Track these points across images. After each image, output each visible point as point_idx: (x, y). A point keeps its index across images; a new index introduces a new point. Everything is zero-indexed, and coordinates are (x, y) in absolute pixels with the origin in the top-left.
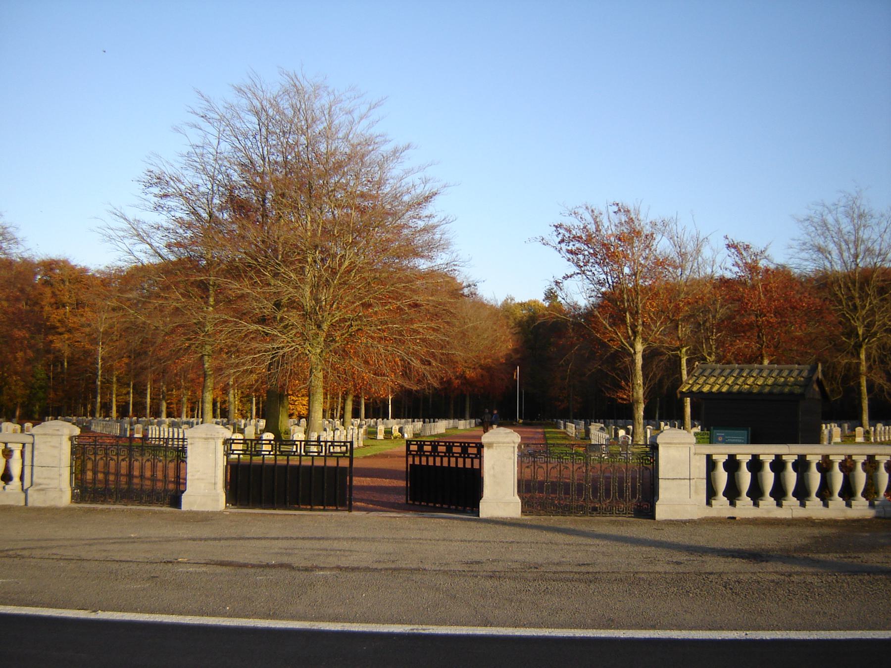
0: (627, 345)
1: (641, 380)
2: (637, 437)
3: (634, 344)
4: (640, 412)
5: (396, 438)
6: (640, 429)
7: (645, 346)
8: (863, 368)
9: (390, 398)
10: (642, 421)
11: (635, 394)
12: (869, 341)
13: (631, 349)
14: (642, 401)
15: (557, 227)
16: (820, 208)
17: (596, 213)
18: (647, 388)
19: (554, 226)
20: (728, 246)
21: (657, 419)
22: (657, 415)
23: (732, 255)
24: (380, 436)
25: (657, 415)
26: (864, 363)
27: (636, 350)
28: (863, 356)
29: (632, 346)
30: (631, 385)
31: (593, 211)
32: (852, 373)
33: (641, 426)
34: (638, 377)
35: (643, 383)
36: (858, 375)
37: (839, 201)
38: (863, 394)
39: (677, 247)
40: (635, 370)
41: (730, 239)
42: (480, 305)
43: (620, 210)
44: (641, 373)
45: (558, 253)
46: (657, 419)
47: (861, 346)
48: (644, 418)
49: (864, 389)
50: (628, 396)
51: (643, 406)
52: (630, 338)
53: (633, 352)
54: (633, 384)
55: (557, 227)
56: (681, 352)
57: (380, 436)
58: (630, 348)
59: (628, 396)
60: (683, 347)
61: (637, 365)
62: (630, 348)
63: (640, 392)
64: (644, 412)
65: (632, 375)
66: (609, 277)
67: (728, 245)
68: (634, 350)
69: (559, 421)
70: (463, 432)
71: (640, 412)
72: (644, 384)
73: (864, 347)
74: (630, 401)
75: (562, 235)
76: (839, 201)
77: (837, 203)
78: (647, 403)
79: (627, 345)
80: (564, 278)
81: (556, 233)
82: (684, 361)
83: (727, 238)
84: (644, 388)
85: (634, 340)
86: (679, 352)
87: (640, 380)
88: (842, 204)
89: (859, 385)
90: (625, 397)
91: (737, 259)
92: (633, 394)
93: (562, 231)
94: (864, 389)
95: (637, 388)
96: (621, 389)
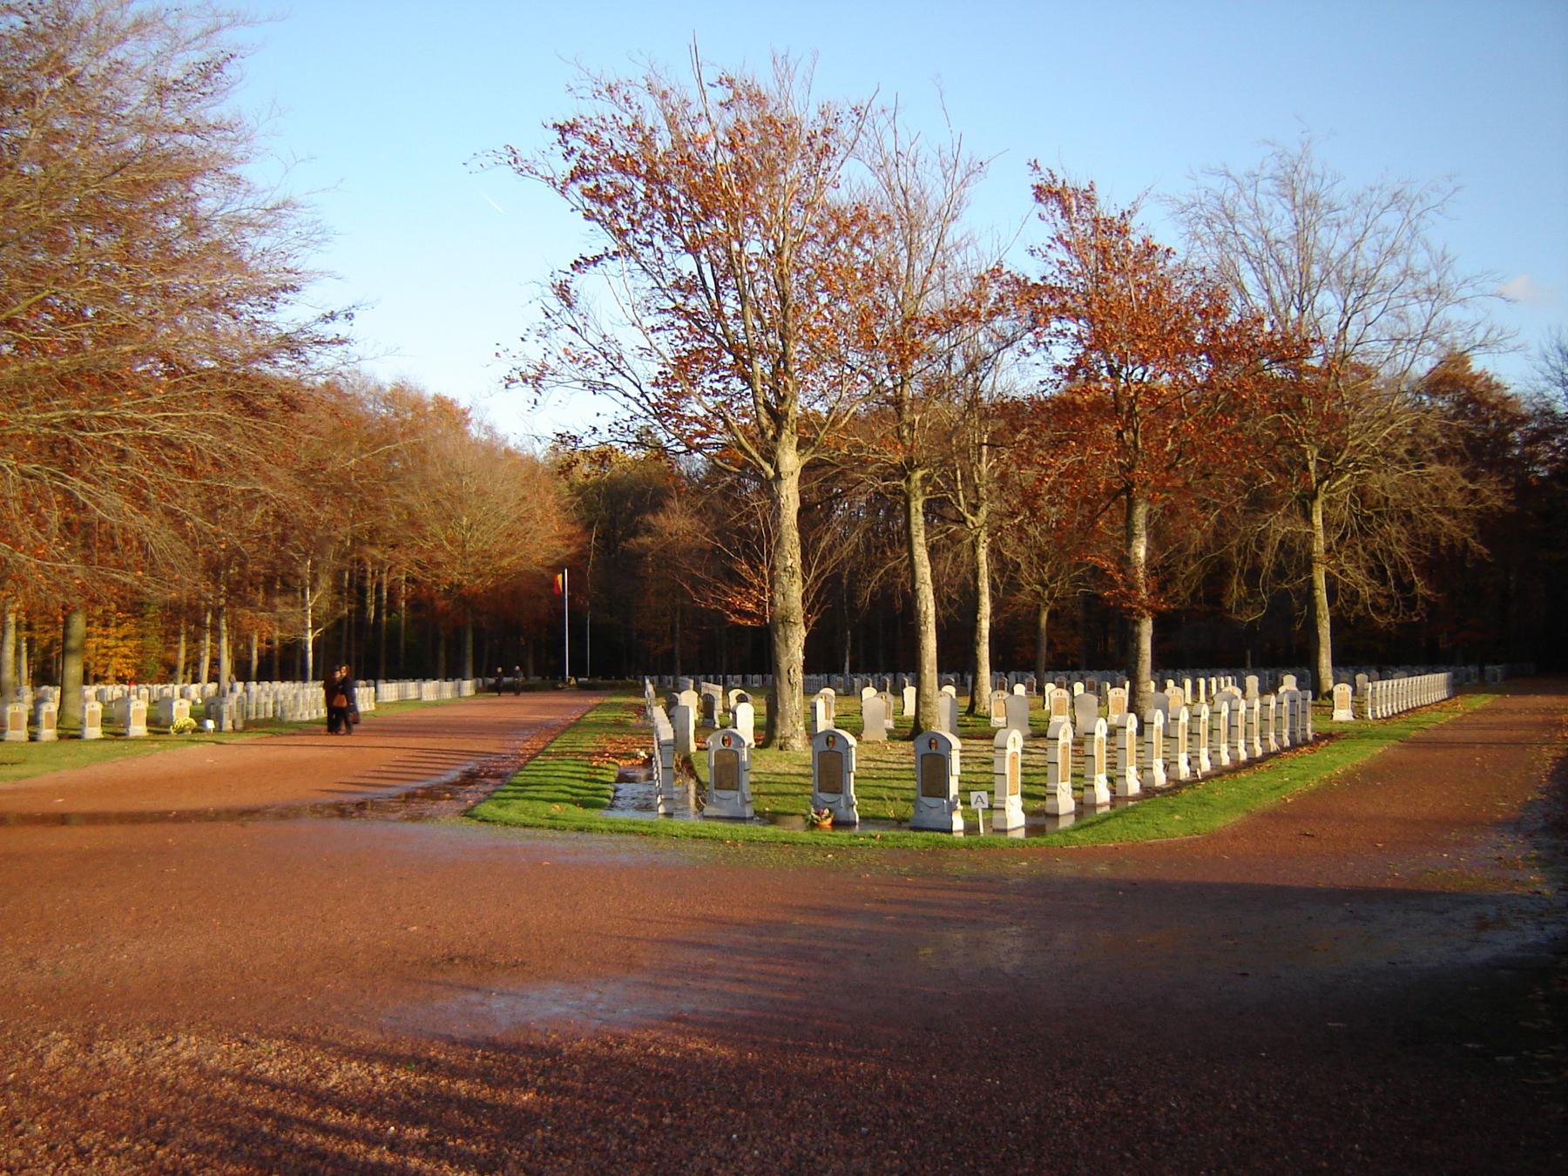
0: (754, 453)
1: (798, 557)
2: (785, 725)
3: (773, 452)
4: (793, 649)
5: (181, 731)
6: (793, 701)
7: (807, 458)
8: (1319, 546)
9: (310, 637)
10: (798, 677)
11: (778, 598)
12: (1330, 485)
13: (767, 467)
14: (801, 620)
15: (562, 130)
16: (1216, 184)
17: (674, 100)
18: (816, 578)
19: (555, 126)
20: (1042, 193)
21: (847, 672)
22: (847, 664)
23: (1048, 217)
24: (138, 728)
25: (847, 664)
26: (1320, 535)
27: (782, 469)
28: (1318, 520)
29: (770, 455)
30: (766, 572)
31: (664, 95)
32: (1296, 558)
33: (798, 691)
34: (788, 547)
35: (803, 566)
36: (1308, 565)
37: (1262, 168)
38: (1320, 607)
39: (898, 192)
40: (779, 526)
41: (1043, 170)
42: (495, 455)
43: (738, 96)
44: (795, 535)
45: (558, 195)
46: (847, 672)
47: (1315, 496)
48: (807, 669)
49: (1321, 595)
50: (759, 604)
51: (804, 633)
52: (763, 432)
53: (772, 473)
54: (773, 568)
55: (562, 130)
56: (908, 480)
57: (138, 728)
58: (763, 463)
59: (759, 604)
60: (913, 469)
61: (784, 512)
62: (763, 463)
63: (793, 593)
64: (806, 651)
65: (769, 542)
66: (707, 269)
67: (1039, 188)
68: (776, 470)
69: (686, 678)
70: (395, 711)
71: (793, 649)
72: (806, 566)
73: (1322, 497)
74: (763, 618)
75: (577, 155)
76: (1262, 168)
77: (1256, 172)
78: (816, 624)
79: (754, 453)
80: (576, 265)
81: (561, 150)
82: (917, 505)
83: (1036, 167)
84: (804, 581)
85: (775, 438)
86: (903, 482)
87: (792, 556)
88: (1267, 172)
89: (1311, 584)
90: (749, 606)
91: (1062, 224)
92: (771, 598)
93: (576, 142)
94: (1321, 595)
95: (785, 580)
96: (740, 585)
